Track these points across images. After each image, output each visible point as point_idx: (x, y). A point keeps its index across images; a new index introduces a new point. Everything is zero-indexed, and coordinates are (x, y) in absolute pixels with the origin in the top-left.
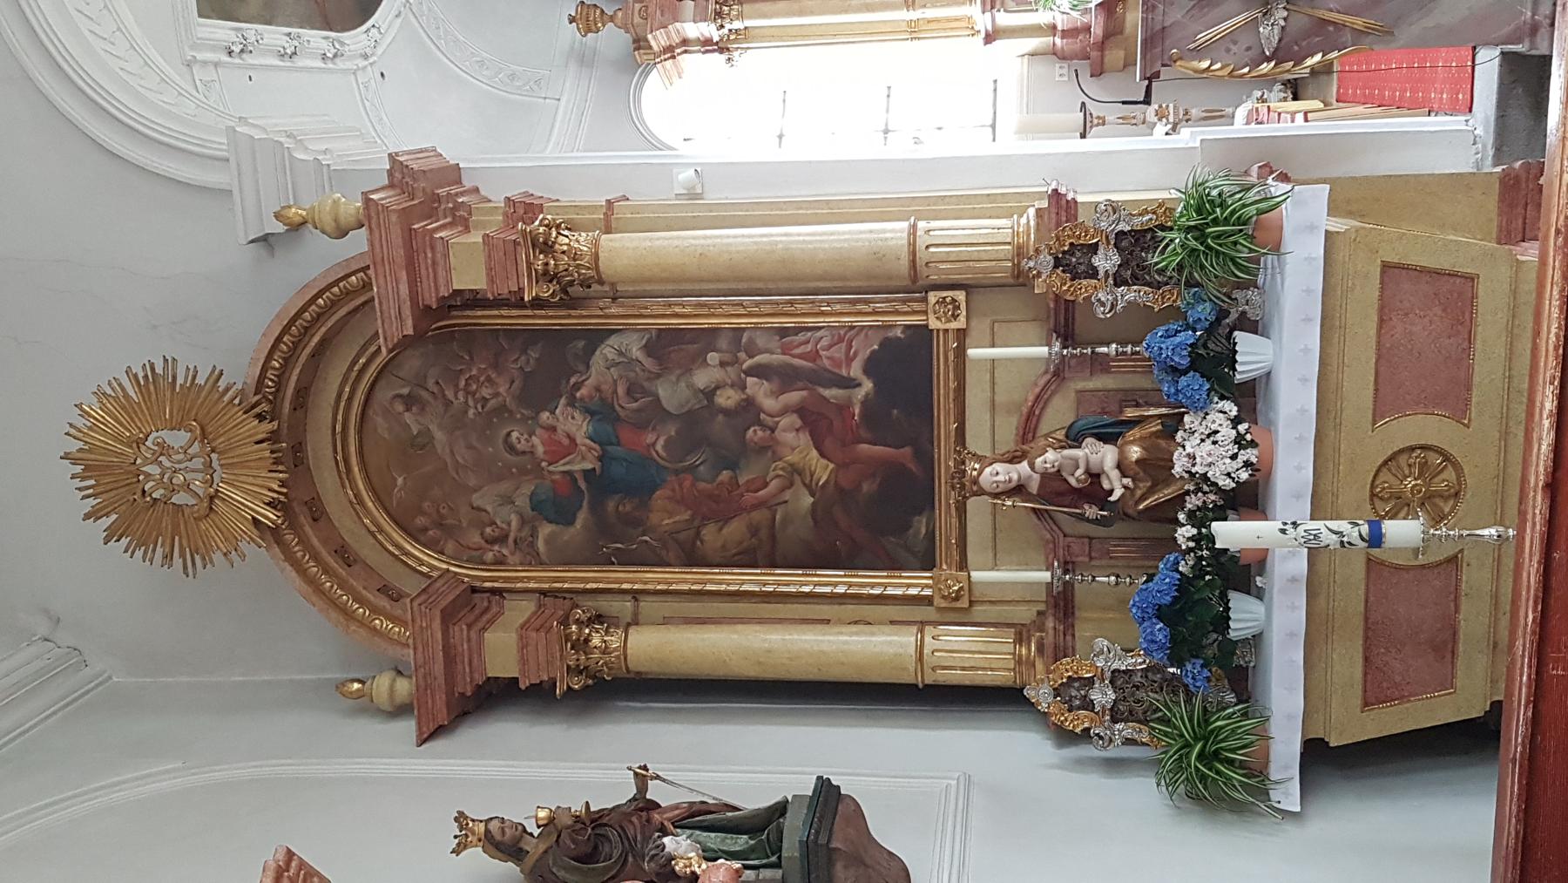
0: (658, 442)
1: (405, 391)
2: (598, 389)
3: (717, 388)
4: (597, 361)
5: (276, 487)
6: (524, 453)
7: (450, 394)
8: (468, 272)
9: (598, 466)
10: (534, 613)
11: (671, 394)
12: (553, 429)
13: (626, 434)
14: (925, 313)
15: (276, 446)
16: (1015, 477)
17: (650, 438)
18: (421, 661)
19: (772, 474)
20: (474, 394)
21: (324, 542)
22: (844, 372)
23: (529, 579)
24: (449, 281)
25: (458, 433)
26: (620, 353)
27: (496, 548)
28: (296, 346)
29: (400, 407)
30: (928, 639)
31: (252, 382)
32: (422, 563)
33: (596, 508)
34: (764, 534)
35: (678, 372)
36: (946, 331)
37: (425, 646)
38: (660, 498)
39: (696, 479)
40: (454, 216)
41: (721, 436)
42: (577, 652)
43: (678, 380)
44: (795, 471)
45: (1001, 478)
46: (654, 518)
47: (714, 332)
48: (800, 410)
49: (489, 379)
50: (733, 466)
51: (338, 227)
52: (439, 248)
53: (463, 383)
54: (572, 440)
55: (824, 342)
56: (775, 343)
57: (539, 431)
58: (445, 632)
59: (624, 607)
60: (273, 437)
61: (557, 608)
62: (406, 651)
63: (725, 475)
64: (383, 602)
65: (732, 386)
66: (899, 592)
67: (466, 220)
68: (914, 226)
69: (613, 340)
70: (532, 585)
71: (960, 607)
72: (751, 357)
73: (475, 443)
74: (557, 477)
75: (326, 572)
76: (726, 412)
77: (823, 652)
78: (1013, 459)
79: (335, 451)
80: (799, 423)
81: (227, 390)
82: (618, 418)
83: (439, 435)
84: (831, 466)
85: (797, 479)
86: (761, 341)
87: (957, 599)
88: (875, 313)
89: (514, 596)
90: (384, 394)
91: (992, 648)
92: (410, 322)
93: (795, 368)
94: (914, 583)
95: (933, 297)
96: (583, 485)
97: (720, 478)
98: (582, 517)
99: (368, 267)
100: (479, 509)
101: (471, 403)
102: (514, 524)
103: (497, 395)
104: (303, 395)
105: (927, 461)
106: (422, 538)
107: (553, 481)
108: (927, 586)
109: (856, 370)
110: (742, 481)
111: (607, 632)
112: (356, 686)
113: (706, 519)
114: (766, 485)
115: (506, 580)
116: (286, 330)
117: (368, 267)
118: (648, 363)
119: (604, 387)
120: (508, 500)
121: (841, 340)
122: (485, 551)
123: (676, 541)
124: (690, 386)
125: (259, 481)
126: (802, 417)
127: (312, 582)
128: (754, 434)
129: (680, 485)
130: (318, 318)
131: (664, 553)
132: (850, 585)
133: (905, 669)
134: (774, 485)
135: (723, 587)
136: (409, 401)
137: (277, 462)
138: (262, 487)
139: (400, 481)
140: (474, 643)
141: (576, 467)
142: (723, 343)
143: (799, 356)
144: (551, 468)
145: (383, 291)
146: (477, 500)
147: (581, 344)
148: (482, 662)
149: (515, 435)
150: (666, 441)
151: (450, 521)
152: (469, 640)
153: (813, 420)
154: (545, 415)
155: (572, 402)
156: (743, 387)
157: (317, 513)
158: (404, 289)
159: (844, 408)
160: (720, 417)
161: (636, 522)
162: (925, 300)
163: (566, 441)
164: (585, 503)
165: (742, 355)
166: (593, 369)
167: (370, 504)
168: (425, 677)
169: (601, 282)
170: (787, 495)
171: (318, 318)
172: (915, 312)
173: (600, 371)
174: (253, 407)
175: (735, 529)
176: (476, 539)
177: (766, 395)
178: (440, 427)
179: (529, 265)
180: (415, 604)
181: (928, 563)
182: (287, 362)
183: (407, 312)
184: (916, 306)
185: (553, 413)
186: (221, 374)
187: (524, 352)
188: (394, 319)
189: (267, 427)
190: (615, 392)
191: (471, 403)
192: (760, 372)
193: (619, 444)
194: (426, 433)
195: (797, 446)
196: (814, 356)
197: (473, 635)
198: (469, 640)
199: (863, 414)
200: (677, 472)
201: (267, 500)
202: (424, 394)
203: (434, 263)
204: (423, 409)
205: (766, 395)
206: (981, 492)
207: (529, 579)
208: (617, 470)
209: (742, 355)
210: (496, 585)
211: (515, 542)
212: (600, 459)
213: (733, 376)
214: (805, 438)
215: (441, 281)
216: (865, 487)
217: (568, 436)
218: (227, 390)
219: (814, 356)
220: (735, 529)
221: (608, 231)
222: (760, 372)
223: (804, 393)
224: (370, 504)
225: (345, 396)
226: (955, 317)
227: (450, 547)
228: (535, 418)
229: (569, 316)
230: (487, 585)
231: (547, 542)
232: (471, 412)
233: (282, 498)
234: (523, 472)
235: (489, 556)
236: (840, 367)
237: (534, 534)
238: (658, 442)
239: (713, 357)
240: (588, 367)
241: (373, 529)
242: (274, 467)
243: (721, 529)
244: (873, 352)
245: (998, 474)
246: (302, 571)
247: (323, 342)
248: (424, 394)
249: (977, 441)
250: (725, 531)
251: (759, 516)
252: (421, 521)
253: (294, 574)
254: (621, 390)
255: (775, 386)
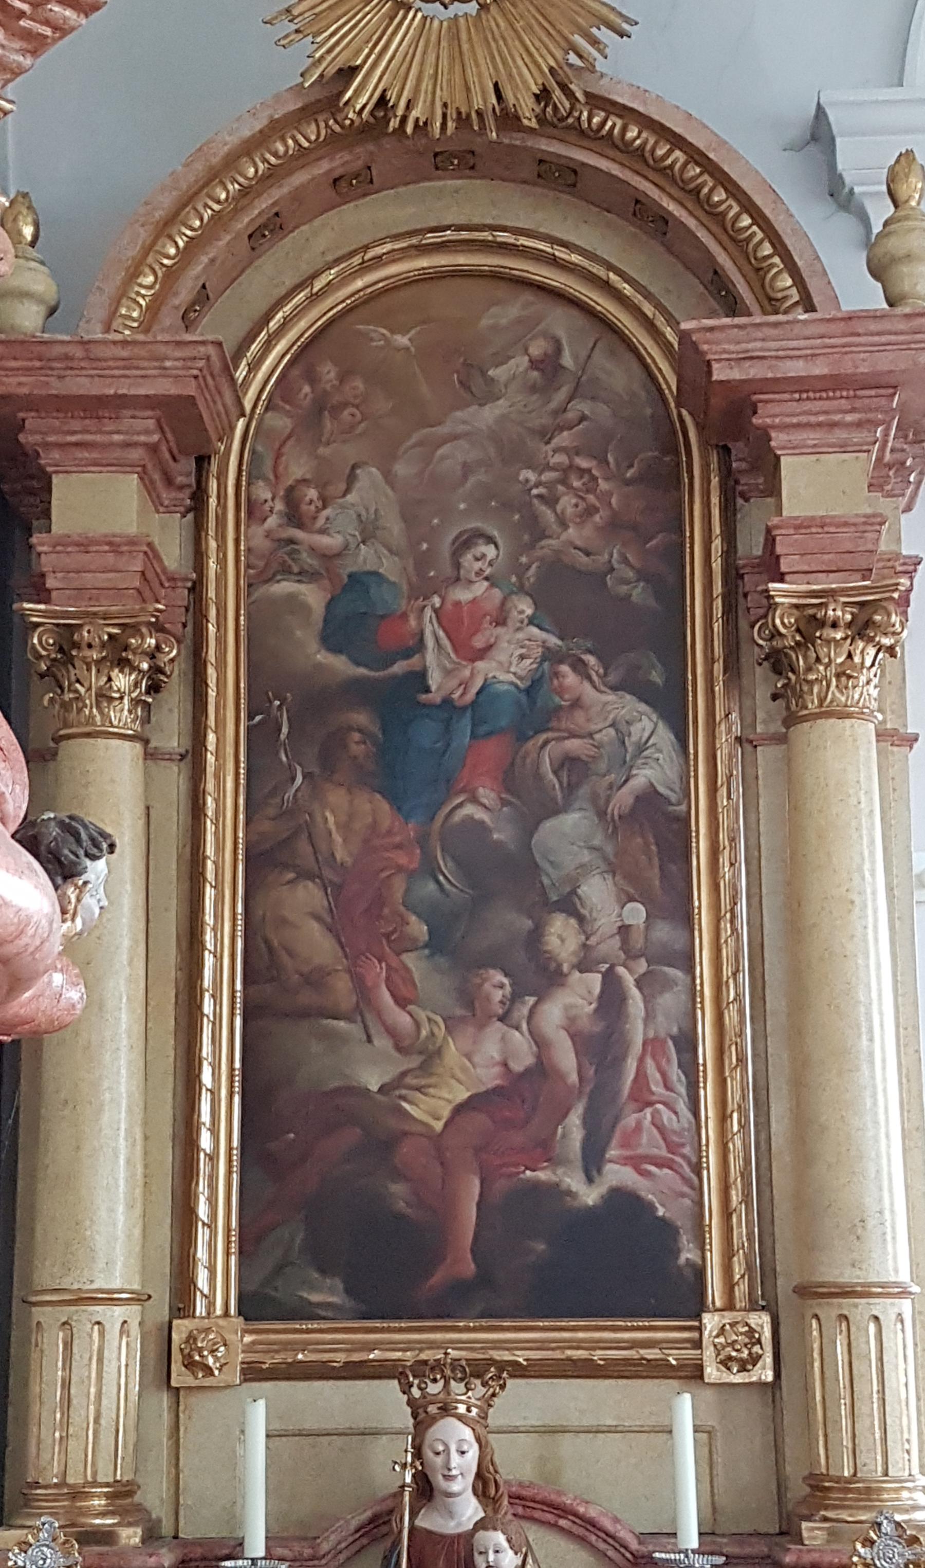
0: (481, 808)
1: (567, 360)
2: (577, 703)
3: (581, 919)
4: (626, 705)
5: (415, 114)
6: (458, 566)
7: (564, 439)
8: (814, 483)
9: (435, 697)
10: (164, 569)
11: (569, 835)
12: (501, 621)
13: (493, 749)
14: (730, 1306)
15: (490, 122)
16: (455, 1487)
17: (487, 795)
18: (100, 351)
19: (422, 1015)
20: (564, 481)
21: (297, 196)
22: (612, 1153)
23: (222, 562)
24: (797, 449)
25: (492, 451)
26: (641, 748)
27: (279, 506)
28: (664, 174)
29: (537, 348)
30: (119, 1312)
31: (602, 88)
32: (253, 367)
33: (357, 693)
34: (307, 998)
35: (609, 849)
36: (698, 1344)
37: (128, 363)
38: (374, 808)
39: (411, 875)
40: (890, 466)
41: (491, 922)
42: (103, 645)
43: (593, 849)
44: (430, 1058)
45: (455, 1459)
46: (337, 797)
47: (687, 919)
48: (542, 1069)
49: (591, 511)
50: (436, 945)
51: (895, 260)
52: (857, 436)
53: (584, 463)
54: (483, 653)
55: (666, 1115)
56: (667, 1026)
57: (497, 594)
58: (150, 402)
59: (172, 738)
60: (508, 119)
61: (168, 604)
62: (99, 327)
63: (419, 929)
64: (185, 293)
65: (584, 946)
66: (202, 1253)
67: (881, 488)
68: (904, 1293)
69: (664, 736)
70: (212, 565)
71: (168, 1364)
72: (639, 983)
73: (472, 480)
74: (413, 622)
75: (245, 192)
76: (536, 936)
77: (100, 1110)
78: (484, 1484)
79: (459, 228)
80: (518, 1067)
81: (595, 42)
82: (523, 738)
83: (487, 416)
84: (438, 1126)
85: (414, 1062)
86: (670, 1001)
87: (190, 1364)
88: (727, 1213)
89: (188, 533)
90: (560, 321)
91: (107, 1440)
92: (736, 374)
93: (620, 1059)
94: (216, 1273)
95: (762, 1321)
96: (399, 668)
97: (413, 918)
98: (341, 665)
99: (810, 307)
100: (351, 479)
101: (548, 476)
102: (325, 541)
103: (564, 525)
104: (562, 178)
105: (445, 1307)
106: (295, 372)
107: (404, 616)
108: (211, 1305)
109: (618, 1174)
110: (409, 959)
111: (136, 702)
112: (28, 232)
113: (335, 890)
114: (402, 1002)
115: (221, 521)
116: (696, 156)
117: (810, 307)
118: (623, 799)
119: (579, 716)
120: (369, 531)
121: (672, 1148)
122: (274, 488)
123: (296, 834)
124: (584, 870)
125: (426, 84)
126: (528, 1071)
127: (231, 162)
128: (496, 985)
129: (399, 846)
130: (715, 217)
131: (271, 811)
132: (213, 1158)
133: (67, 1269)
134: (402, 1019)
135: (209, 919)
136: (548, 367)
137: (463, 120)
138: (417, 89)
139: (402, 340)
140: (118, 453)
141: (430, 657)
142: (664, 932)
143: (641, 1075)
144: (428, 612)
145: (797, 329)
146: (369, 476)
147: (657, 677)
148: (83, 466)
149: (490, 551)
150: (482, 823)
151: (328, 424)
152: (127, 445)
153: (522, 1096)
154: (526, 607)
155: (550, 656)
156: (584, 966)
157: (348, 186)
158: (796, 369)
159: (546, 1151)
160: (529, 924)
161: (329, 761)
162: (753, 1307)
163: (479, 642)
164: (362, 671)
165: (642, 966)
166: (611, 697)
167: (359, 284)
168: (67, 357)
169: (791, 720)
170: (382, 1042)
171: (715, 217)
172: (730, 1286)
173: (609, 711)
174: (564, 88)
175: (315, 944)
176: (297, 468)
177: (567, 1008)
178: (503, 418)
179: (831, 594)
180: (211, 350)
181: (253, 1306)
182: (637, 157)
183: (754, 371)
184: (742, 1290)
185: (531, 621)
186: (622, 34)
187: (642, 575)
188: (736, 351)
189: (527, 108)
190: (573, 735)
191: (548, 476)
192: (612, 1000)
193: (473, 736)
194: (490, 395)
195: (478, 1061)
196: (642, 1098)
197: (136, 454)
198: (127, 445)
199: (536, 1187)
200: (423, 840)
201: (392, 96)
202: (561, 395)
203: (833, 425)
204: (533, 389)
205: (567, 1008)
206: (423, 1418)
207: (222, 562)
208: (426, 733)
209: (642, 966)
210: (213, 502)
211: (291, 541)
212: (447, 701)
213: (604, 948)
214: (489, 1077)
215: (798, 436)
216: (398, 1189)
217: (490, 647)
218: (595, 42)
219: (642, 1098)
220: (315, 944)
221: (880, 735)
222: (612, 1000)
223: (573, 1078)
224: (359, 284)
225: (561, 253)
226: (726, 1363)
227: (280, 422)
228: (521, 589)
229: (710, 660)
230: (213, 485)
231: (291, 598)
232: (530, 475)
233: (394, 124)
234: (423, 562)
235: (263, 492)
236: (625, 1145)
237: (304, 575)
238: (481, 808)
239: (636, 914)
240: (614, 688)
241: (318, 285)
242: (452, 113)
243: (318, 918)
244: (651, 1207)
245: (458, 1448)
246: (249, 148)
247: (664, 220)
248: (561, 395)
249: (523, 1401)
250: (315, 925)
251: (342, 988)
252: (328, 372)
253: (247, 133)
254: (573, 745)
255: (585, 1024)
